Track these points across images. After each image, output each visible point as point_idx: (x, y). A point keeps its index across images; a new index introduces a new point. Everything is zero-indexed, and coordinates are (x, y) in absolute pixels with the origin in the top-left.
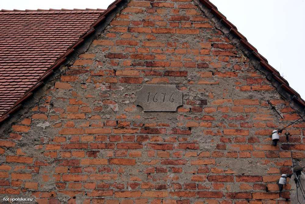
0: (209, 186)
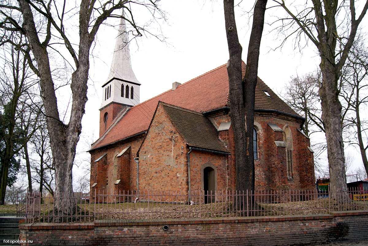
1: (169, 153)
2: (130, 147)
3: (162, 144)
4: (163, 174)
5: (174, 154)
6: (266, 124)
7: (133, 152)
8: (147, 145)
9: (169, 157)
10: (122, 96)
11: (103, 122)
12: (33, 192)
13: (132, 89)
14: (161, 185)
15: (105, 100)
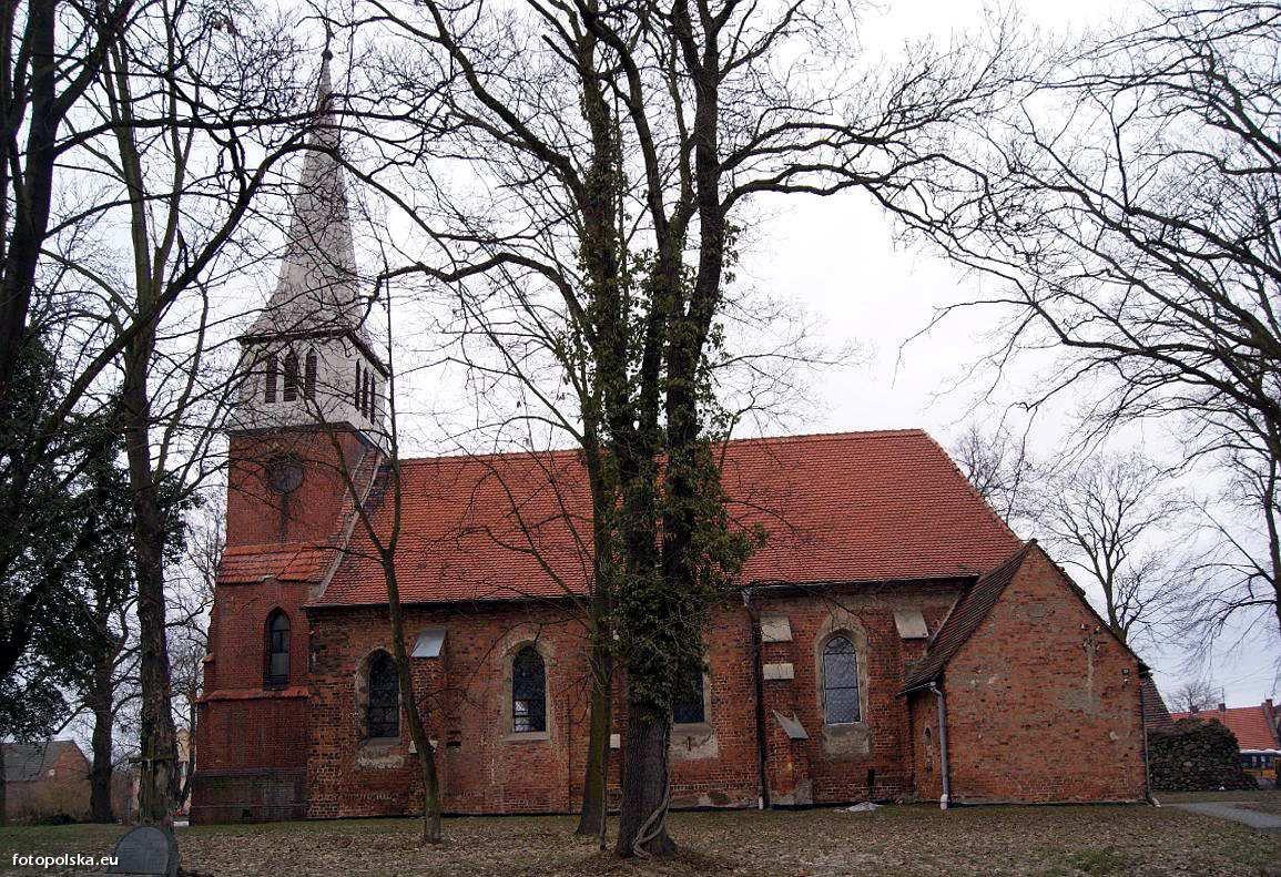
0: (1057, 648)
4: (1055, 733)
5: (1096, 682)
12: (672, 764)
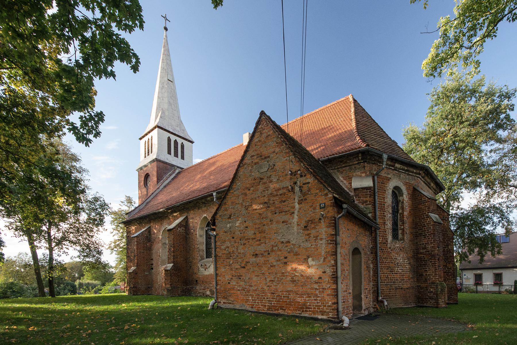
1: (285, 217)
2: (187, 217)
3: (269, 200)
4: (272, 259)
5: (300, 218)
6: (412, 187)
7: (191, 225)
8: (232, 203)
9: (287, 226)
10: (169, 152)
11: (144, 186)
13: (183, 146)
14: (268, 280)
15: (145, 157)
